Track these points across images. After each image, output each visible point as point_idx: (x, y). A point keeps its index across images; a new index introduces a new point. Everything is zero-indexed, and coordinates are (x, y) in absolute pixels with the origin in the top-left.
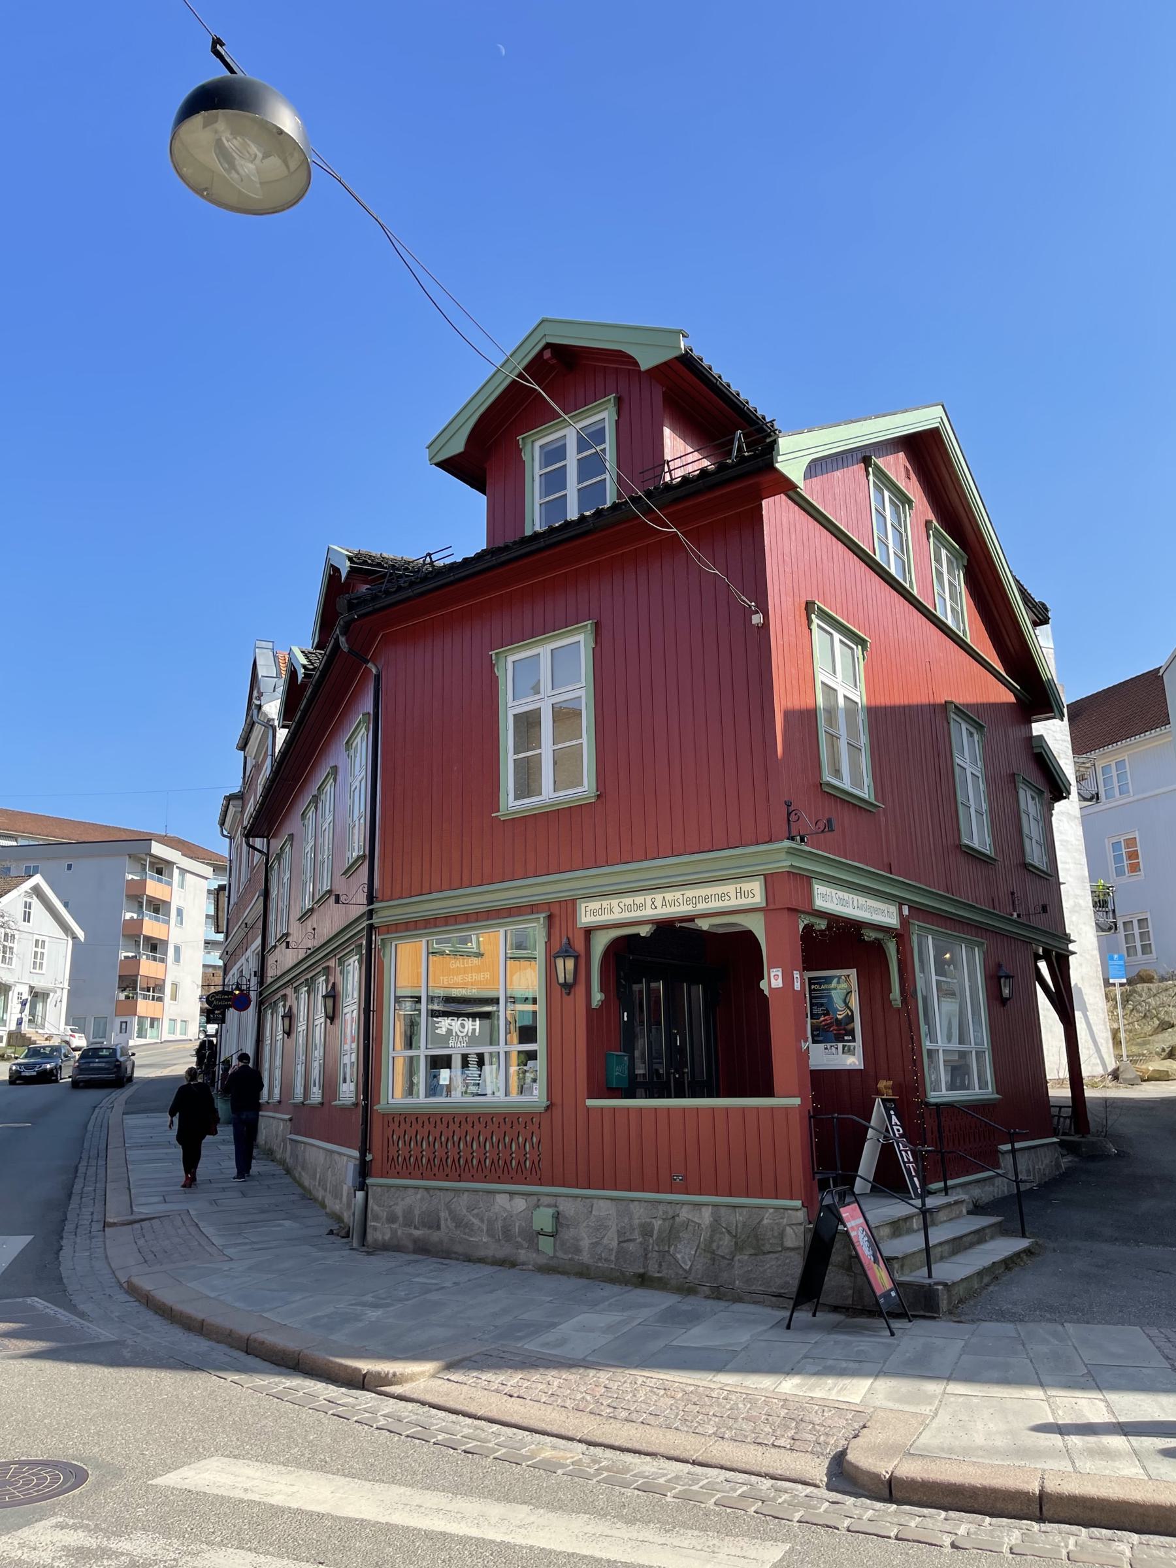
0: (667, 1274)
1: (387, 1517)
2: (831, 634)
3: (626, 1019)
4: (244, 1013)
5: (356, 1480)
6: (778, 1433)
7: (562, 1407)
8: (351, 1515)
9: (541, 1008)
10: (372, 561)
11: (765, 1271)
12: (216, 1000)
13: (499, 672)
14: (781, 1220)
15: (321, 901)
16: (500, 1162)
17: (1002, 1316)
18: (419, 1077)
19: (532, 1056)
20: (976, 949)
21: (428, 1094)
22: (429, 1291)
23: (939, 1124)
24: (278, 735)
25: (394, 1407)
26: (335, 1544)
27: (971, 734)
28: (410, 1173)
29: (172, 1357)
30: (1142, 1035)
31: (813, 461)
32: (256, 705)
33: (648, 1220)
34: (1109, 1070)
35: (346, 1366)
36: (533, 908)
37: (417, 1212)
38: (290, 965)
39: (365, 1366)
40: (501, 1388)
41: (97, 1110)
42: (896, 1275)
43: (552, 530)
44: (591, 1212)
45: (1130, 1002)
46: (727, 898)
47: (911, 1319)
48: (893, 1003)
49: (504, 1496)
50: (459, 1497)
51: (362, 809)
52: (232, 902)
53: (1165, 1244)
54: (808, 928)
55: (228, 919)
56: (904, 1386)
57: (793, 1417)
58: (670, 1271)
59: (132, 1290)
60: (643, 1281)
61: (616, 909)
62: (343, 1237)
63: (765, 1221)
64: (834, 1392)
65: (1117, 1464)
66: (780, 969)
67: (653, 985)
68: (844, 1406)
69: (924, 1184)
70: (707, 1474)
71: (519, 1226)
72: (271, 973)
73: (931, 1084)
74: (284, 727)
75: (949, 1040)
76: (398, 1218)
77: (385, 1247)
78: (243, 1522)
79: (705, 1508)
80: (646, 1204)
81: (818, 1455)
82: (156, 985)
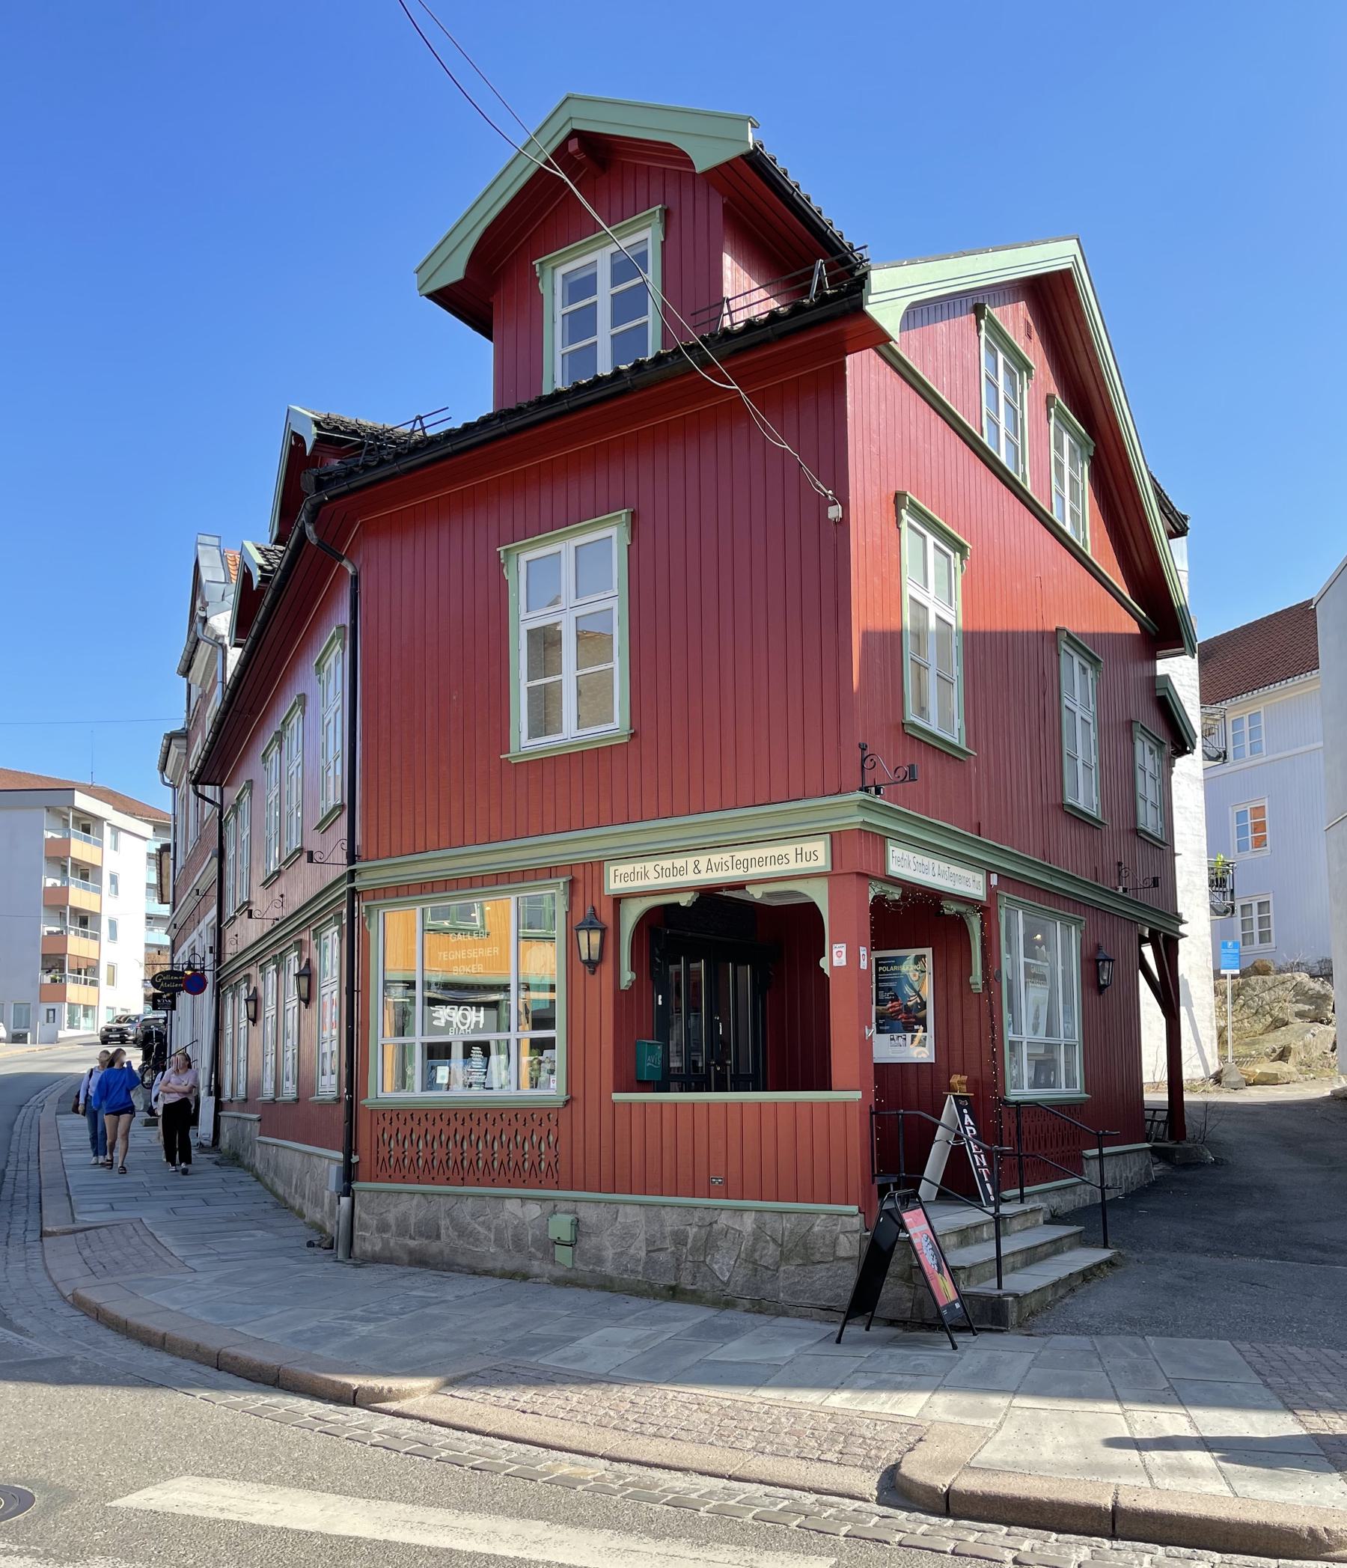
0: (702, 1286)
1: (385, 1534)
2: (924, 536)
3: (660, 1003)
4: (198, 997)
5: (349, 1498)
6: (825, 1447)
7: (582, 1422)
8: (344, 1532)
9: (559, 997)
10: (346, 427)
11: (814, 1282)
12: (164, 981)
13: (509, 575)
14: (834, 1227)
15: (290, 861)
16: (511, 1163)
17: (1077, 1329)
18: (414, 1068)
19: (549, 1043)
20: (1073, 927)
21: (425, 1087)
22: (429, 1304)
23: (1019, 1124)
24: (229, 657)
25: (391, 1424)
26: (326, 1563)
27: (1084, 670)
28: (404, 1177)
29: (130, 1374)
30: (1252, 1034)
31: (914, 306)
32: (201, 618)
33: (682, 1228)
34: (1212, 1073)
35: (334, 1382)
36: (551, 872)
37: (412, 1220)
38: (254, 938)
39: (355, 1382)
40: (513, 1404)
41: (24, 1110)
42: (962, 1285)
43: (578, 388)
44: (616, 1218)
45: (1242, 997)
46: (786, 861)
47: (976, 1332)
48: (973, 987)
49: (517, 1512)
50: (467, 1513)
51: (339, 747)
52: (178, 866)
53: (1263, 1256)
54: (879, 900)
55: (174, 886)
56: (966, 1400)
57: (841, 1430)
58: (706, 1283)
59: (79, 1303)
60: (674, 1293)
61: (652, 874)
62: (326, 1248)
63: (816, 1229)
64: (887, 1406)
65: (1200, 1481)
66: (845, 945)
67: (692, 966)
68: (898, 1420)
69: (996, 1193)
70: (744, 1489)
71: (532, 1235)
72: (230, 950)
73: (1012, 1080)
74: (236, 645)
75: (1035, 1030)
76: (391, 1226)
77: (375, 1259)
78: (219, 1543)
79: (742, 1522)
80: (680, 1210)
81: (868, 1469)
82: (89, 967)
